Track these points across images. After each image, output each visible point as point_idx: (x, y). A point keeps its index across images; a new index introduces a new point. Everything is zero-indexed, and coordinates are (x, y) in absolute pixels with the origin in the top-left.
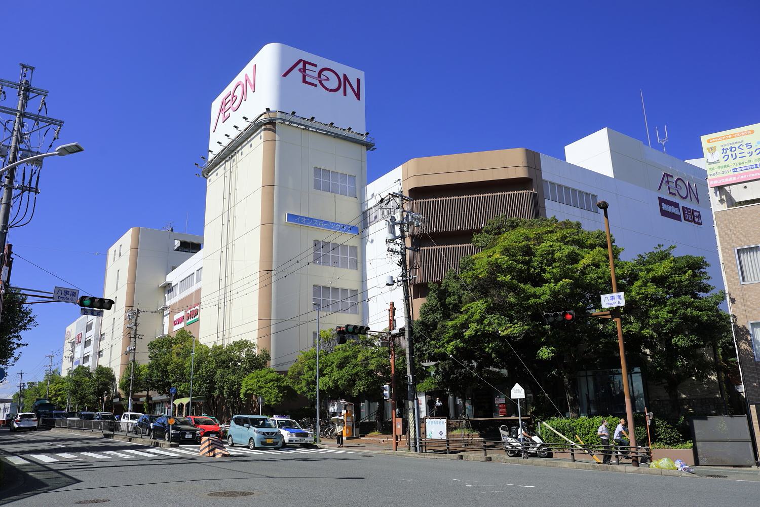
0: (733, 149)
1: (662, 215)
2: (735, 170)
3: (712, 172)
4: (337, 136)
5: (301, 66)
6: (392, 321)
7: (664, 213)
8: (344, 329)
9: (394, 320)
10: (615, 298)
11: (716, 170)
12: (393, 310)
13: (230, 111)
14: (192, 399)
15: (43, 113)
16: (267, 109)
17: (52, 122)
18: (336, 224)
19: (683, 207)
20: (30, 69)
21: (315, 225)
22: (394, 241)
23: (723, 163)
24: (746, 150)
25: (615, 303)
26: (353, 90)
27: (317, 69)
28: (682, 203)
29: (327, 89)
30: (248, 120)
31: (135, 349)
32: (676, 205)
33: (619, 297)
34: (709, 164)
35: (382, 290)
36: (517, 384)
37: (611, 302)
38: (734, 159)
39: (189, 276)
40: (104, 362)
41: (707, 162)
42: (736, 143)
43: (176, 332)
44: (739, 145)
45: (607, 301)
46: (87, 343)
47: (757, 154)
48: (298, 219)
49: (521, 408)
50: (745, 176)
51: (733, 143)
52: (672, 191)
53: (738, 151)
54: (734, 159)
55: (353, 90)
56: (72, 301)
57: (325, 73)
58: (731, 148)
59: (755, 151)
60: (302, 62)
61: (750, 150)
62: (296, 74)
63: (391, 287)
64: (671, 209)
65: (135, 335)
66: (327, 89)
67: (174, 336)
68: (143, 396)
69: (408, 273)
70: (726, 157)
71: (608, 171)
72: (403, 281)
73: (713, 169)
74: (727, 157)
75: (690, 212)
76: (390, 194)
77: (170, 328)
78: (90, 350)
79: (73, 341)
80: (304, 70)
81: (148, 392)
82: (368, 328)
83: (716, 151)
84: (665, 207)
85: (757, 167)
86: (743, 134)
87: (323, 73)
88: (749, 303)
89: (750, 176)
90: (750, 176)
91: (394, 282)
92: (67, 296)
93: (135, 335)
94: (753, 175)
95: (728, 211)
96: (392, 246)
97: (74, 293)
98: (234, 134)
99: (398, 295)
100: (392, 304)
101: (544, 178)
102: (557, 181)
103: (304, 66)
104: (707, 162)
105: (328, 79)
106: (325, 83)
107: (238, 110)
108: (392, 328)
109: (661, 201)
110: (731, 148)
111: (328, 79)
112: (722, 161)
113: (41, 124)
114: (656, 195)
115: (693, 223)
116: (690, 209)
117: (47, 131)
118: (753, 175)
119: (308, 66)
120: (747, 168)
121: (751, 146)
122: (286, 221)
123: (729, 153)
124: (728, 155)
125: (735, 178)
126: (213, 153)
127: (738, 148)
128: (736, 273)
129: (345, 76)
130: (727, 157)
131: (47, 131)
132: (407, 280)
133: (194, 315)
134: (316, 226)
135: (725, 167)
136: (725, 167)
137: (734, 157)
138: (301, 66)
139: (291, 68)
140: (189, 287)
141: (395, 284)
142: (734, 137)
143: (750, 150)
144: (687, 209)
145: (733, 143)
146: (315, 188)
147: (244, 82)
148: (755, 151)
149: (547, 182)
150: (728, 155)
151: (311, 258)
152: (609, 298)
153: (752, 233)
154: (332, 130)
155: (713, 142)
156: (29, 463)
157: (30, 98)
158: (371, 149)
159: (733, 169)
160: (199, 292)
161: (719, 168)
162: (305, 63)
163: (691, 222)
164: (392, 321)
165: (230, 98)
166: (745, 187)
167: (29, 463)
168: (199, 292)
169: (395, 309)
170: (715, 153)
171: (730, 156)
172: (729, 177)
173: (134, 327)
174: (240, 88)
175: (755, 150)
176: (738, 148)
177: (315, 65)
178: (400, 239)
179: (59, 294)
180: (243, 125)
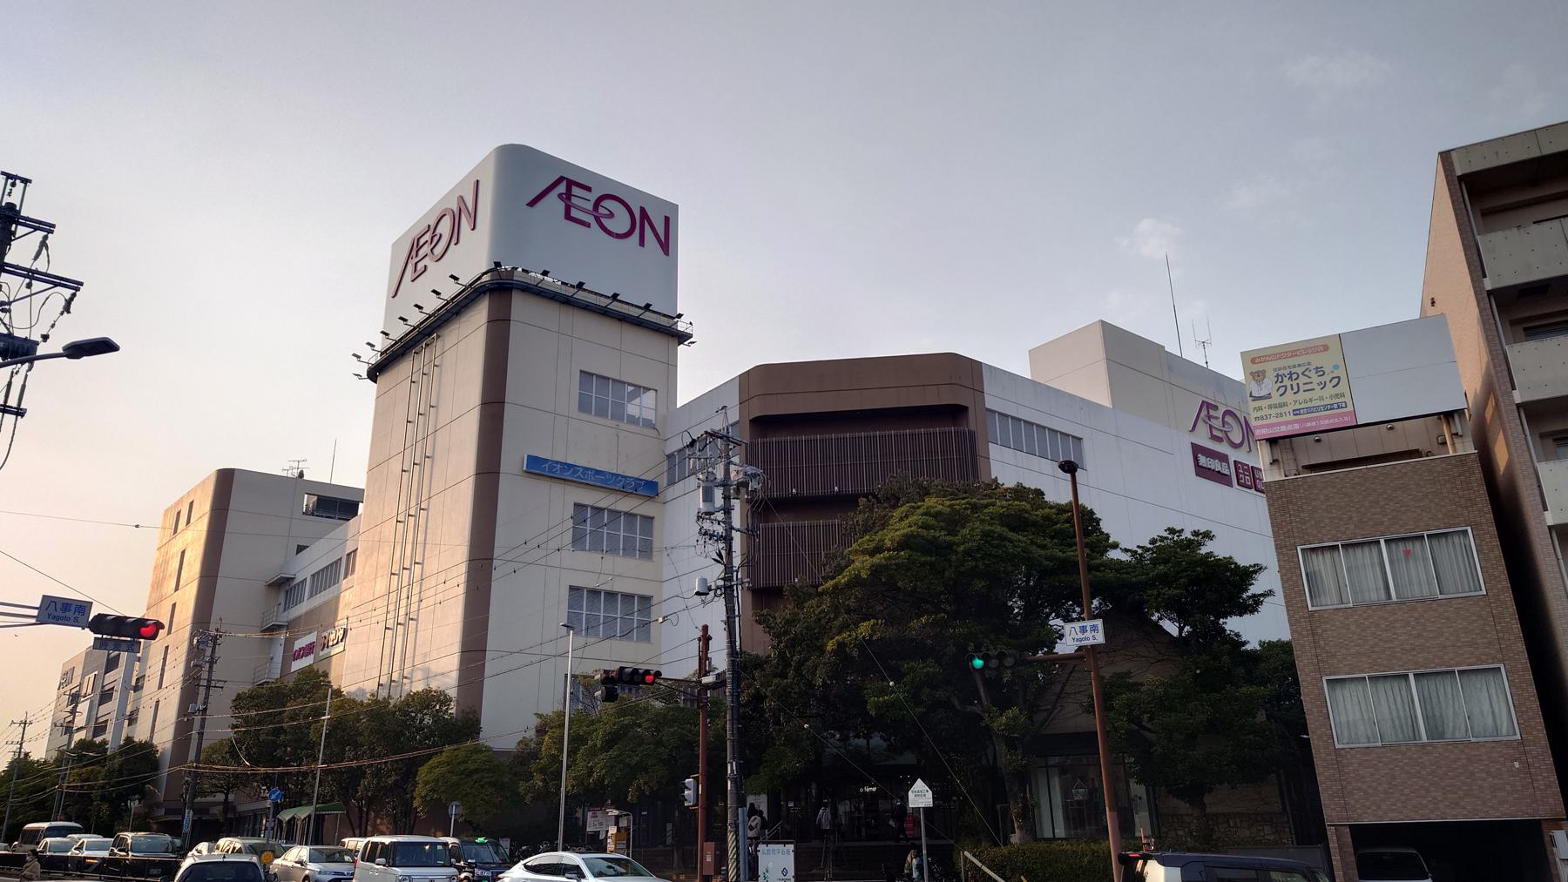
0: (1294, 376)
1: (1198, 474)
2: (1296, 412)
3: (1259, 414)
4: (623, 319)
5: (562, 188)
6: (704, 658)
7: (1202, 471)
8: (614, 674)
10: (1088, 629)
11: (1266, 412)
12: (706, 639)
13: (426, 261)
14: (316, 810)
15: (41, 265)
17: (57, 281)
18: (617, 475)
19: (1235, 461)
20: (22, 182)
22: (712, 517)
23: (1276, 399)
24: (1315, 379)
26: (657, 235)
27: (593, 196)
28: (1234, 455)
29: (609, 233)
30: (375, 348)
32: (1223, 458)
33: (1094, 628)
34: (1253, 401)
35: (690, 603)
36: (919, 780)
37: (1080, 636)
38: (1295, 393)
40: (141, 734)
41: (1251, 396)
42: (1299, 365)
43: (296, 675)
44: (1303, 369)
46: (106, 696)
47: (1334, 387)
49: (926, 825)
50: (1314, 424)
51: (1294, 366)
52: (1216, 433)
53: (1302, 379)
54: (1295, 393)
55: (657, 235)
56: (75, 623)
58: (1291, 374)
59: (1330, 381)
60: (565, 182)
61: (1323, 379)
62: (553, 203)
63: (703, 597)
64: (1215, 465)
65: (209, 681)
66: (609, 233)
67: (290, 682)
68: (218, 804)
69: (735, 574)
70: (1282, 390)
72: (725, 587)
73: (1260, 409)
74: (1284, 388)
75: (1248, 470)
76: (706, 433)
77: (286, 664)
78: (111, 707)
79: (73, 691)
80: (567, 197)
81: (227, 795)
82: (658, 674)
83: (1266, 379)
84: (1203, 460)
85: (1333, 409)
86: (1310, 351)
88: (1322, 643)
89: (1322, 422)
90: (1322, 422)
91: (710, 589)
92: (68, 614)
93: (209, 681)
94: (1327, 422)
95: (1286, 483)
96: (707, 525)
97: (84, 607)
98: (432, 305)
99: (714, 613)
100: (705, 628)
104: (1251, 396)
105: (611, 215)
106: (605, 222)
107: (441, 260)
108: (703, 672)
109: (1197, 450)
110: (1291, 374)
111: (611, 215)
112: (1275, 395)
113: (37, 286)
114: (1188, 440)
115: (1253, 491)
116: (1246, 465)
117: (47, 299)
118: (1327, 422)
119: (575, 190)
120: (1317, 409)
121: (1324, 373)
122: (525, 469)
123: (1287, 382)
124: (1286, 386)
125: (1297, 426)
126: (375, 348)
127: (1303, 374)
128: (1300, 591)
130: (1284, 388)
131: (47, 299)
132: (732, 586)
135: (1281, 405)
136: (1281, 405)
137: (1295, 390)
138: (562, 188)
139: (551, 190)
140: (329, 587)
141: (712, 593)
142: (1296, 355)
143: (1323, 379)
144: (1243, 464)
145: (1294, 366)
148: (1330, 381)
150: (1286, 386)
151: (568, 537)
152: (1078, 630)
153: (1327, 521)
154: (615, 306)
155: (1260, 362)
157: (17, 236)
158: (686, 343)
159: (1294, 411)
161: (1270, 407)
162: (570, 183)
163: (1250, 488)
164: (704, 658)
165: (427, 237)
166: (1318, 441)
169: (710, 638)
170: (1265, 381)
171: (1289, 388)
172: (1286, 423)
173: (208, 665)
175: (1330, 378)
176: (1303, 374)
177: (588, 189)
179: (51, 610)
180: (450, 290)
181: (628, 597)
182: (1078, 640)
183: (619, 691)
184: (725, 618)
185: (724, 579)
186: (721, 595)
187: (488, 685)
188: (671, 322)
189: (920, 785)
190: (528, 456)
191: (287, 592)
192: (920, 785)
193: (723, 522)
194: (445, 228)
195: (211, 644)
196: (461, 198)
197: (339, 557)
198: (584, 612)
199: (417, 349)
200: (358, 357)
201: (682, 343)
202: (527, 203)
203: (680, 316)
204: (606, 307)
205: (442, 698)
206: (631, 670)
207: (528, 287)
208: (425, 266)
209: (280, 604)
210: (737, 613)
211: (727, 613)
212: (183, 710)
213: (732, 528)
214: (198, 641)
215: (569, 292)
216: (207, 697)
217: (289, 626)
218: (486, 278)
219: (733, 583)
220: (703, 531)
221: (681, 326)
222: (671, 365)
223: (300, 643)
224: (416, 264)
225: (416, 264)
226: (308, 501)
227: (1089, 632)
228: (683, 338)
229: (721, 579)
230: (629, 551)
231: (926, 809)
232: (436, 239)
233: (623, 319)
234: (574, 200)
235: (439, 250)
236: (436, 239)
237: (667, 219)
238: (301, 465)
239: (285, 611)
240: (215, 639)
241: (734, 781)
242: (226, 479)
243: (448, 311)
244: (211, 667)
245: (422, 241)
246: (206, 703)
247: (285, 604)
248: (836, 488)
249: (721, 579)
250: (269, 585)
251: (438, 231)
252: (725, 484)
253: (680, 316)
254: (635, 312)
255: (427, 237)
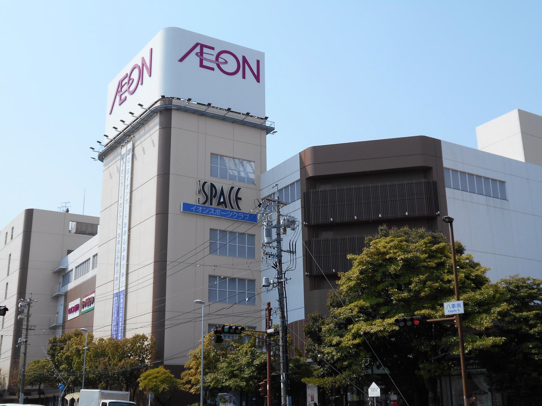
4: (234, 121)
5: (198, 49)
9: (270, 320)
10: (456, 305)
12: (269, 310)
13: (127, 94)
16: (162, 96)
21: (212, 214)
22: (271, 245)
25: (455, 311)
27: (215, 53)
31: (26, 341)
33: (459, 305)
39: (83, 263)
45: (449, 309)
48: (194, 208)
57: (223, 56)
62: (193, 58)
65: (27, 326)
69: (283, 275)
71: (518, 155)
81: (40, 385)
87: (221, 56)
93: (27, 326)
96: (268, 250)
98: (129, 120)
101: (445, 165)
102: (460, 168)
103: (202, 50)
105: (226, 62)
106: (222, 66)
108: (268, 327)
111: (226, 62)
119: (205, 50)
122: (182, 210)
129: (244, 58)
133: (89, 304)
134: (213, 215)
138: (198, 49)
141: (271, 286)
146: (211, 176)
147: (140, 65)
149: (449, 169)
152: (451, 306)
154: (230, 115)
156: (246, 63)
158: (272, 133)
160: (94, 279)
162: (202, 46)
165: (126, 80)
167: (246, 63)
168: (94, 279)
169: (271, 309)
173: (26, 318)
174: (136, 72)
177: (213, 48)
178: (276, 242)
180: (138, 111)
181: (242, 280)
182: (451, 311)
183: (223, 337)
184: (278, 299)
185: (278, 278)
186: (276, 286)
187: (167, 332)
188: (262, 121)
189: (374, 385)
190: (183, 203)
191: (63, 276)
192: (374, 385)
193: (277, 248)
194: (135, 75)
195: (27, 307)
196: (143, 59)
197: (89, 257)
198: (218, 289)
199: (123, 144)
200: (93, 149)
201: (269, 133)
202: (178, 60)
203: (266, 118)
204: (224, 116)
205: (144, 338)
206: (228, 327)
207: (180, 108)
208: (126, 97)
209: (60, 283)
210: (285, 296)
211: (279, 296)
212: (15, 341)
213: (282, 251)
214: (21, 305)
215: (203, 108)
216: (27, 335)
217: (66, 295)
218: (158, 104)
219: (282, 280)
220: (265, 253)
221: (268, 124)
222: (263, 147)
223: (71, 305)
224: (121, 95)
225: (121, 95)
226: (72, 226)
227: (456, 307)
228: (269, 130)
229: (276, 278)
230: (242, 254)
231: (377, 398)
232: (131, 82)
233: (234, 121)
234: (205, 56)
235: (132, 88)
236: (131, 82)
237: (258, 62)
238: (67, 205)
239: (63, 286)
240: (29, 304)
241: (284, 383)
242: (29, 213)
243: (138, 123)
244: (28, 319)
245: (123, 83)
246: (26, 338)
247: (63, 283)
248: (355, 217)
249: (276, 278)
250: (54, 272)
251: (132, 77)
252: (278, 227)
253: (266, 118)
254: (241, 117)
255: (126, 80)
